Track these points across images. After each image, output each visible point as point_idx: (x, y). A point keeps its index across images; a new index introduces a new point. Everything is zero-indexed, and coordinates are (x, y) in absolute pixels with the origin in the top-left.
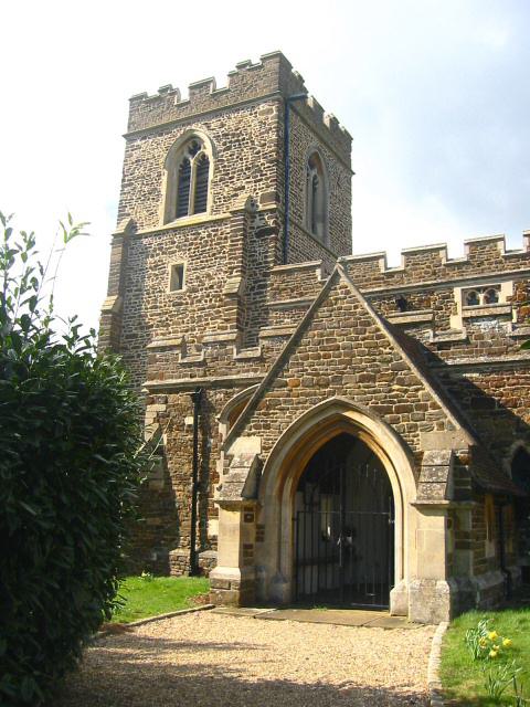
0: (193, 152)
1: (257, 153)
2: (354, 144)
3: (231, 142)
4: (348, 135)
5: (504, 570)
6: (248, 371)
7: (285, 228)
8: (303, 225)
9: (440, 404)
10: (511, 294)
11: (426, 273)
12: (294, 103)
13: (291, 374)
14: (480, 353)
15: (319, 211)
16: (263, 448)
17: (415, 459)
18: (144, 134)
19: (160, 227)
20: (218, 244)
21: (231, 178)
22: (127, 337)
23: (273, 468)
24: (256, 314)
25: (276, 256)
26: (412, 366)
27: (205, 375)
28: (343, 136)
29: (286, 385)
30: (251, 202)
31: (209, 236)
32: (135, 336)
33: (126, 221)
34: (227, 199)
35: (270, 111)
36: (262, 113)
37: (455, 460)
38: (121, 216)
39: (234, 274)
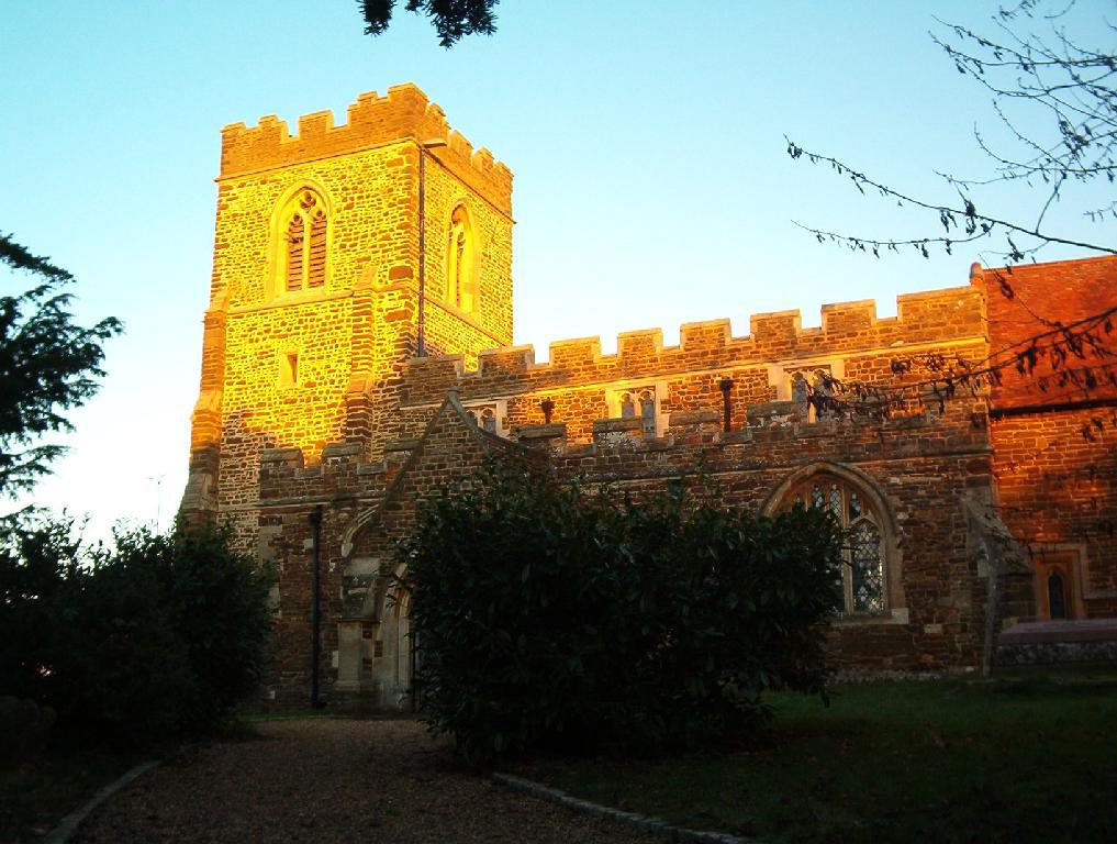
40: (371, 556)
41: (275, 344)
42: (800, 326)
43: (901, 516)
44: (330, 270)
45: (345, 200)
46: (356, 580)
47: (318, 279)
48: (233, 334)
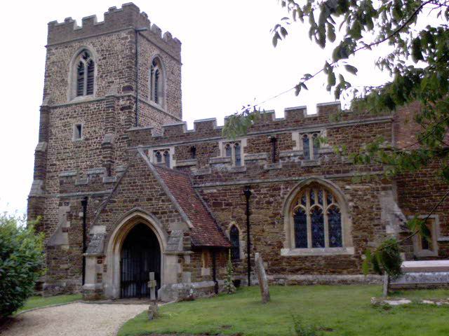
2: (182, 47)
4: (179, 41)
5: (214, 280)
7: (136, 105)
11: (206, 133)
14: (216, 181)
15: (160, 90)
18: (57, 46)
22: (51, 165)
24: (121, 153)
28: (176, 43)
29: (115, 202)
32: (55, 165)
36: (123, 39)
40: (102, 224)
41: (72, 121)
42: (306, 113)
43: (351, 204)
44: (95, 88)
45: (102, 55)
46: (95, 236)
47: (90, 92)
48: (53, 116)
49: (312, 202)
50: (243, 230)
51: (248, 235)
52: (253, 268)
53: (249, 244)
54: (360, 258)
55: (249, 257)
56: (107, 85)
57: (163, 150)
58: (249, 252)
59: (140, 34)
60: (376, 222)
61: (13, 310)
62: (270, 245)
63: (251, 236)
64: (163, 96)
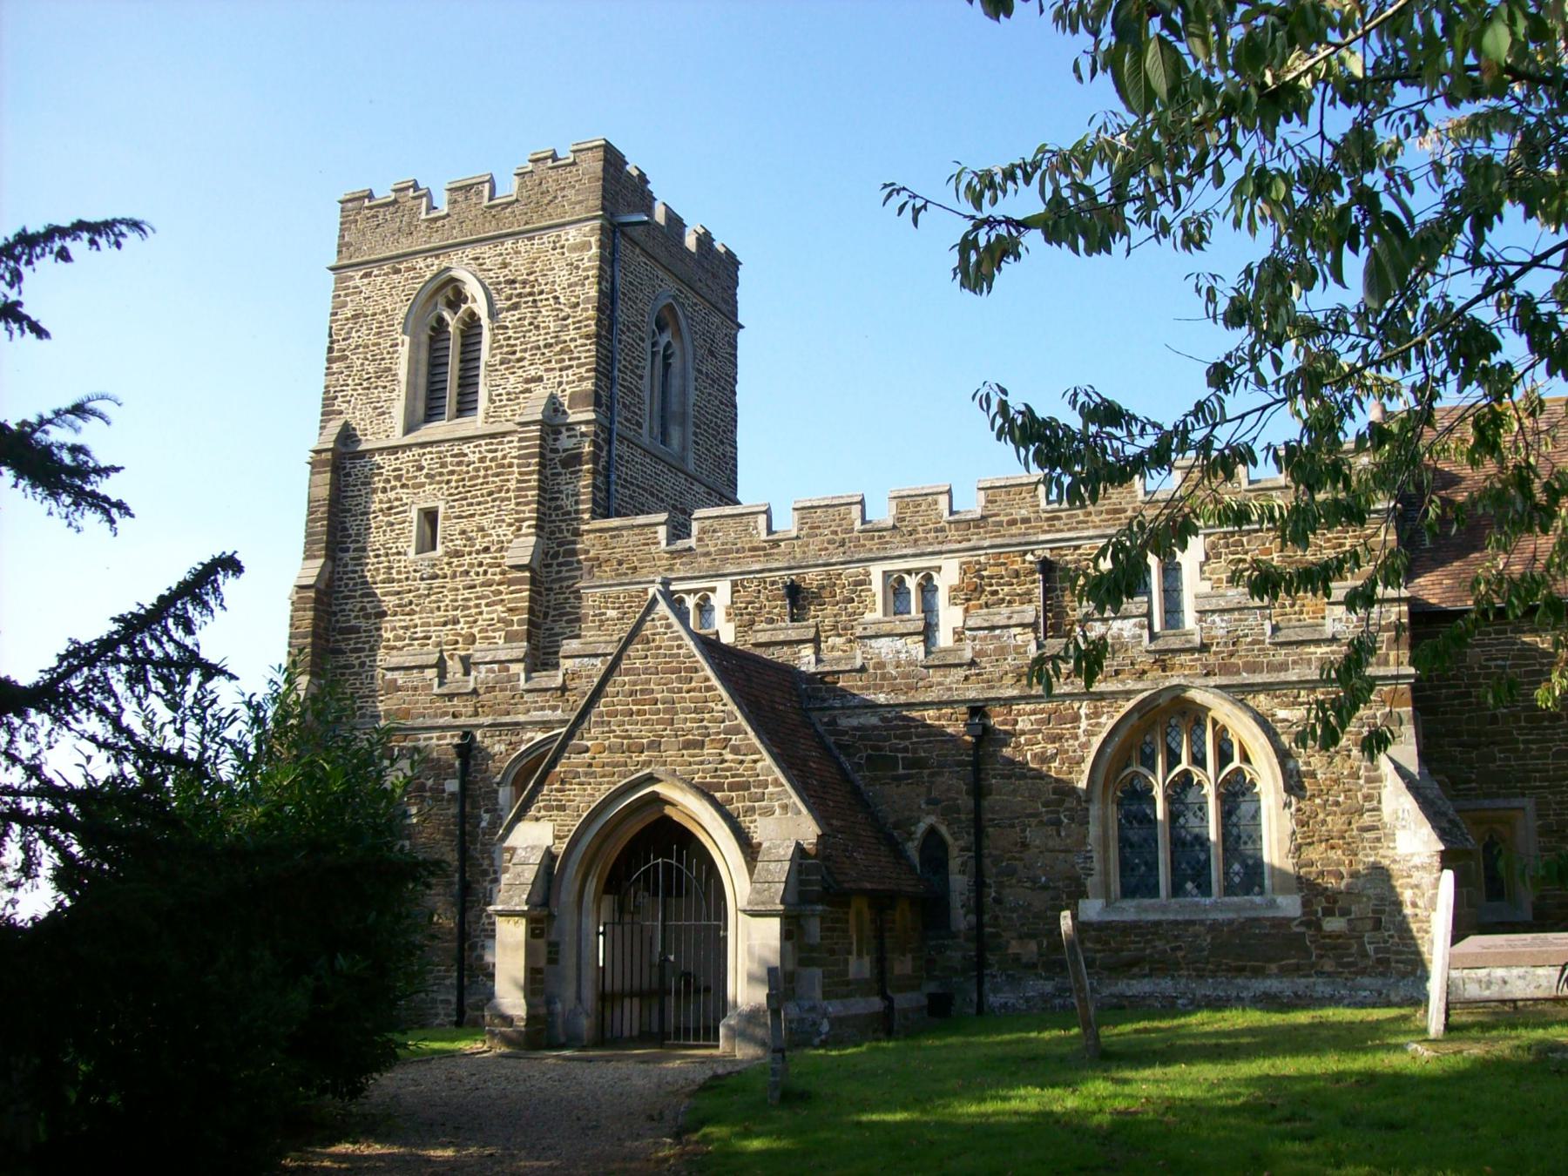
0: (453, 305)
1: (564, 319)
3: (520, 296)
6: (542, 708)
7: (609, 451)
8: (646, 440)
9: (783, 780)
10: (956, 581)
12: (628, 230)
13: (592, 737)
15: (675, 406)
16: (557, 837)
17: (750, 850)
19: (397, 438)
20: (498, 475)
21: (519, 360)
23: (570, 863)
25: (594, 501)
26: (749, 729)
27: (476, 714)
29: (587, 750)
30: (554, 406)
31: (482, 460)
32: (356, 630)
33: (335, 427)
34: (512, 397)
35: (586, 246)
36: (574, 249)
37: (800, 850)
38: (328, 413)
39: (524, 531)
49: (1173, 759)
50: (962, 843)
51: (979, 857)
52: (991, 958)
53: (979, 884)
54: (1319, 928)
55: (980, 925)
56: (521, 387)
57: (695, 592)
58: (979, 910)
59: (624, 234)
60: (1367, 819)
61: (378, 1071)
62: (1045, 888)
63: (987, 861)
64: (683, 424)
